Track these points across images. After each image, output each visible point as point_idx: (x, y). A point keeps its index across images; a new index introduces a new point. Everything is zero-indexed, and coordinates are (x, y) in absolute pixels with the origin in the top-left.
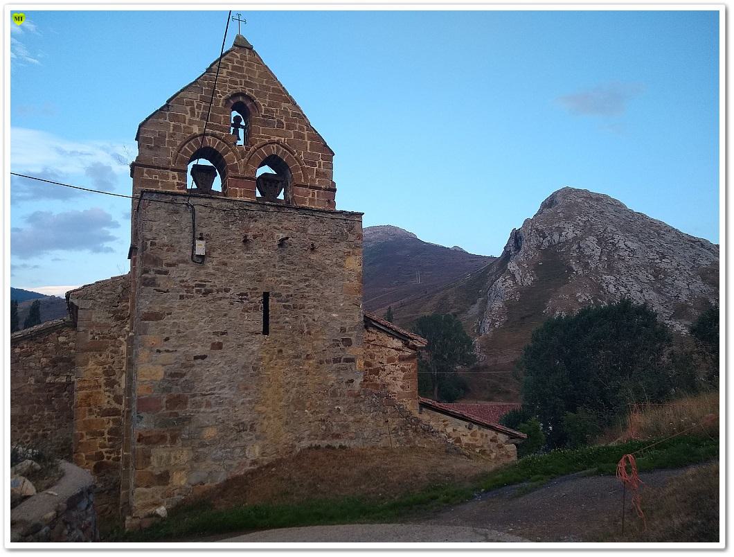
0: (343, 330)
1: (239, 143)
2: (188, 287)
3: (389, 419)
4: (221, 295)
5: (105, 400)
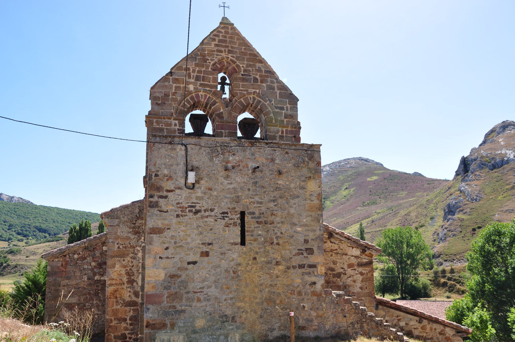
0: (306, 241)
1: (224, 96)
2: (182, 207)
3: (347, 315)
5: (127, 295)
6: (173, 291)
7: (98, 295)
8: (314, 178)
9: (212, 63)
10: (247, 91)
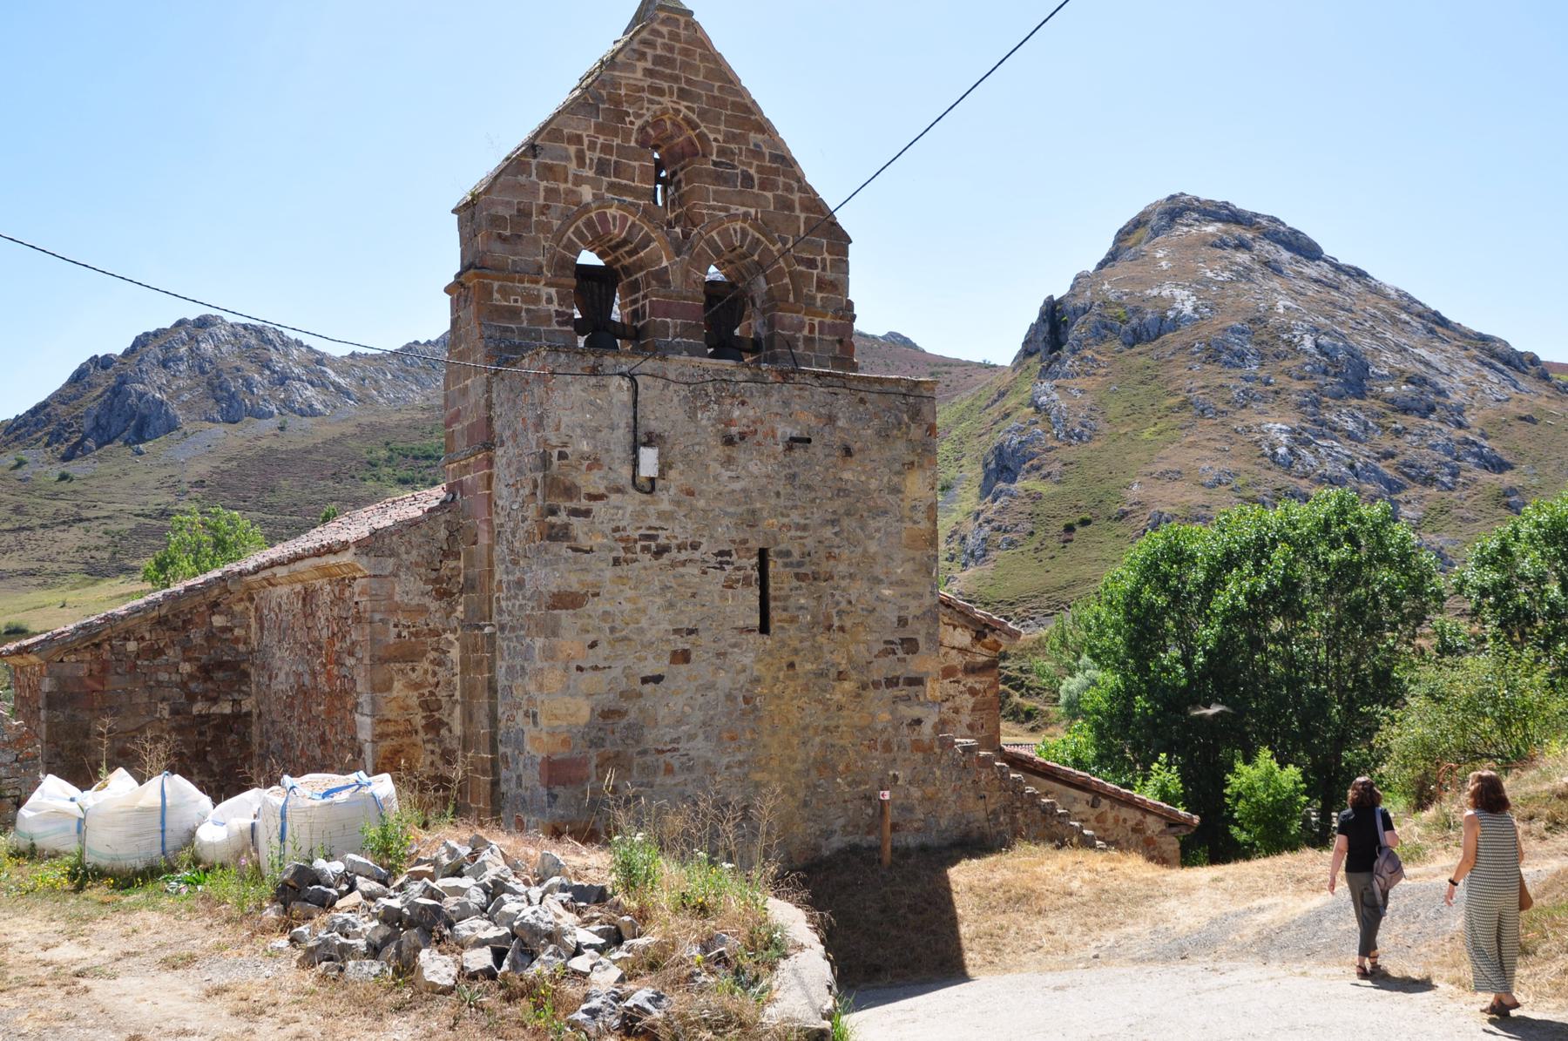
0: (902, 622)
2: (626, 540)
4: (684, 555)
6: (609, 749)
7: (205, 759)
8: (921, 466)
9: (639, 123)
10: (726, 210)
